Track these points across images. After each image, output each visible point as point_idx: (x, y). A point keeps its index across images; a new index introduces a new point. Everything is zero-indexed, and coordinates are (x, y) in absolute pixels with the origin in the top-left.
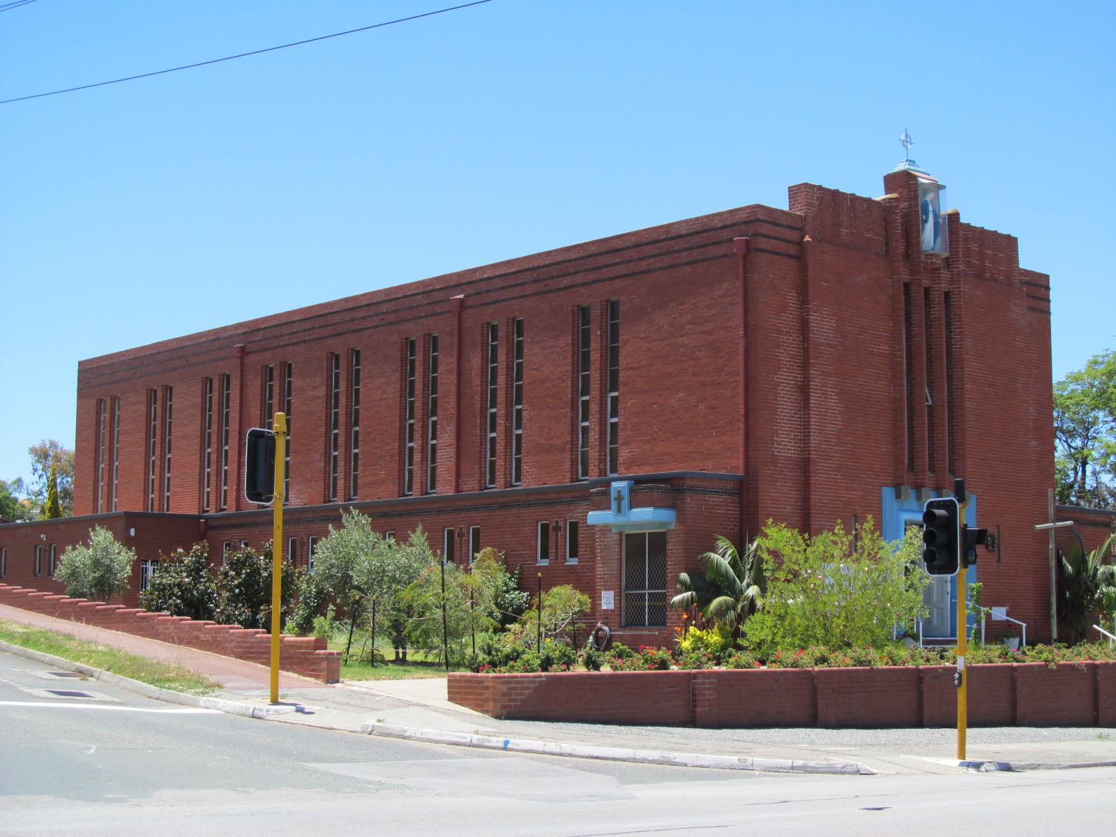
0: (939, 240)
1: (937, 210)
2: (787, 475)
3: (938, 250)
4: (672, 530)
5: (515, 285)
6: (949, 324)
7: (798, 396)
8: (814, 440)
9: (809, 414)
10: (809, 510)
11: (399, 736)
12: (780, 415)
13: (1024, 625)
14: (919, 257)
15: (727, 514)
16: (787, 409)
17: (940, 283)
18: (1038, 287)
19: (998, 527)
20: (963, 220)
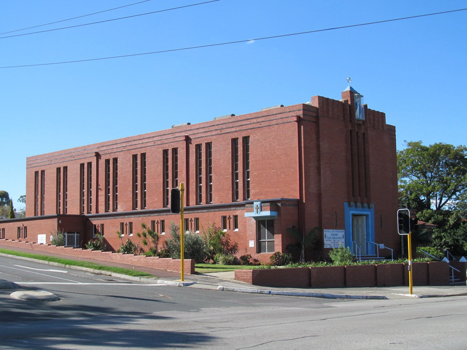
0: (361, 115)
1: (360, 104)
2: (313, 199)
3: (361, 118)
4: (276, 219)
5: (208, 131)
6: (364, 145)
7: (317, 171)
8: (323, 186)
9: (321, 177)
10: (321, 211)
11: (233, 291)
12: (311, 178)
13: (392, 250)
14: (355, 121)
15: (294, 213)
16: (313, 176)
17: (361, 130)
18: (392, 129)
19: (381, 216)
20: (368, 108)
